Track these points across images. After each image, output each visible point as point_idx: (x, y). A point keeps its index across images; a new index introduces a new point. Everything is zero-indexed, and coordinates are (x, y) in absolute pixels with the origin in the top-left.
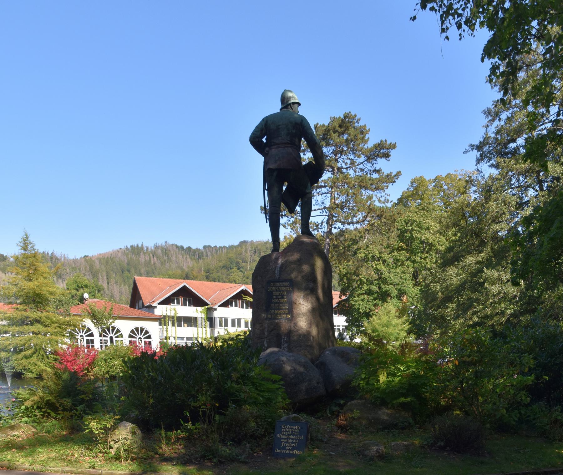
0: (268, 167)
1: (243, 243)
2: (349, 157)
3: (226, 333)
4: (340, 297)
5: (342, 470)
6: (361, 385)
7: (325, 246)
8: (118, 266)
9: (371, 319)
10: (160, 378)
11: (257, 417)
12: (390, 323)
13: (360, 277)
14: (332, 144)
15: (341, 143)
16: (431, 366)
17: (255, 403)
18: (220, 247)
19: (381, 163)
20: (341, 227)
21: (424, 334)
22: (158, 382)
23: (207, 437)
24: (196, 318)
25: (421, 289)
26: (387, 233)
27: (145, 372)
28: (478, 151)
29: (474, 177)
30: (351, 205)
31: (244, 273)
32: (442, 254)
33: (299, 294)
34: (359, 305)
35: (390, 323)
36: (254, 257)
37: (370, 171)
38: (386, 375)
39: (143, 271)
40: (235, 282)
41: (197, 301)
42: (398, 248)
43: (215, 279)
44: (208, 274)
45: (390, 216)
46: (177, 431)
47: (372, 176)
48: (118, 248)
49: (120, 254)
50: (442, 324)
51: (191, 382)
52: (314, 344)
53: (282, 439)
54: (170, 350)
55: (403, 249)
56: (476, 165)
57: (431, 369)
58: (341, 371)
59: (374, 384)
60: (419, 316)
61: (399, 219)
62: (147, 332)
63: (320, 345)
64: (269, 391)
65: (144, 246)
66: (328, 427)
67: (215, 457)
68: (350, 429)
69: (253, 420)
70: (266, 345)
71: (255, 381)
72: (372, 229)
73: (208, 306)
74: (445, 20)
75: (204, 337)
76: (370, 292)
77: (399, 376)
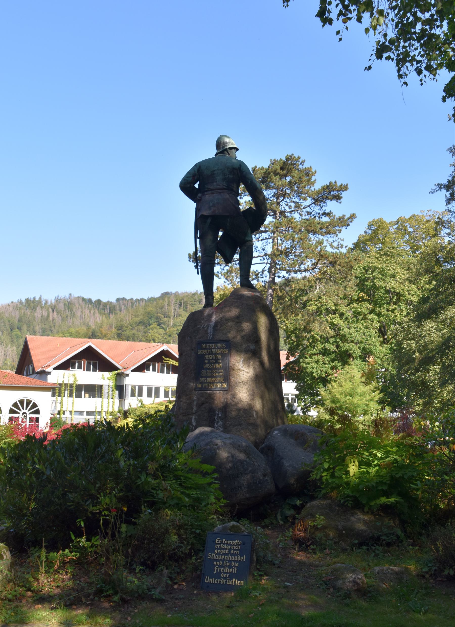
0: (200, 214)
1: (166, 294)
2: (293, 200)
3: (140, 404)
4: (287, 358)
5: (305, 613)
6: (325, 478)
7: (267, 297)
8: (7, 323)
9: (329, 385)
10: (49, 472)
11: (180, 527)
12: (355, 391)
13: (312, 333)
14: (273, 187)
15: (284, 186)
16: (419, 452)
17: (178, 506)
18: (138, 300)
19: (330, 206)
20: (287, 275)
21: (401, 405)
22: (45, 477)
23: (108, 559)
24: (101, 387)
25: (391, 348)
26: (344, 281)
27: (29, 464)
28: (448, 191)
29: (446, 218)
30: (297, 251)
31: (165, 330)
32: (414, 306)
33: (238, 358)
34: (313, 368)
35: (355, 391)
36: (179, 311)
37: (319, 214)
38: (357, 464)
39: (37, 328)
40: (154, 341)
41: (105, 365)
42: (358, 299)
43: (129, 337)
44: (120, 331)
45: (346, 262)
46: (64, 550)
47: (321, 220)
48: (9, 302)
49: (11, 309)
50: (424, 392)
51: (92, 477)
52: (259, 422)
53: (216, 560)
54: (66, 431)
55: (364, 300)
56: (446, 205)
57: (419, 456)
58: (296, 458)
59: (341, 477)
60: (392, 381)
61: (357, 265)
62: (35, 405)
63: (265, 423)
64: (198, 487)
65: (42, 299)
66: (280, 541)
67: (116, 593)
68: (312, 544)
69: (174, 531)
70: (194, 424)
71: (179, 473)
72: (325, 278)
73: (118, 371)
74: (402, 66)
75: (110, 410)
76: (325, 352)
77: (375, 466)
